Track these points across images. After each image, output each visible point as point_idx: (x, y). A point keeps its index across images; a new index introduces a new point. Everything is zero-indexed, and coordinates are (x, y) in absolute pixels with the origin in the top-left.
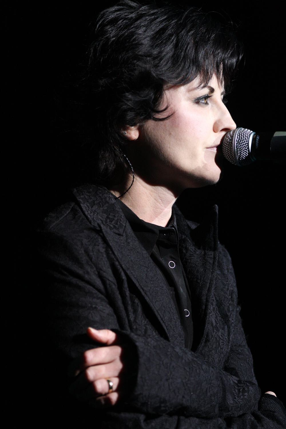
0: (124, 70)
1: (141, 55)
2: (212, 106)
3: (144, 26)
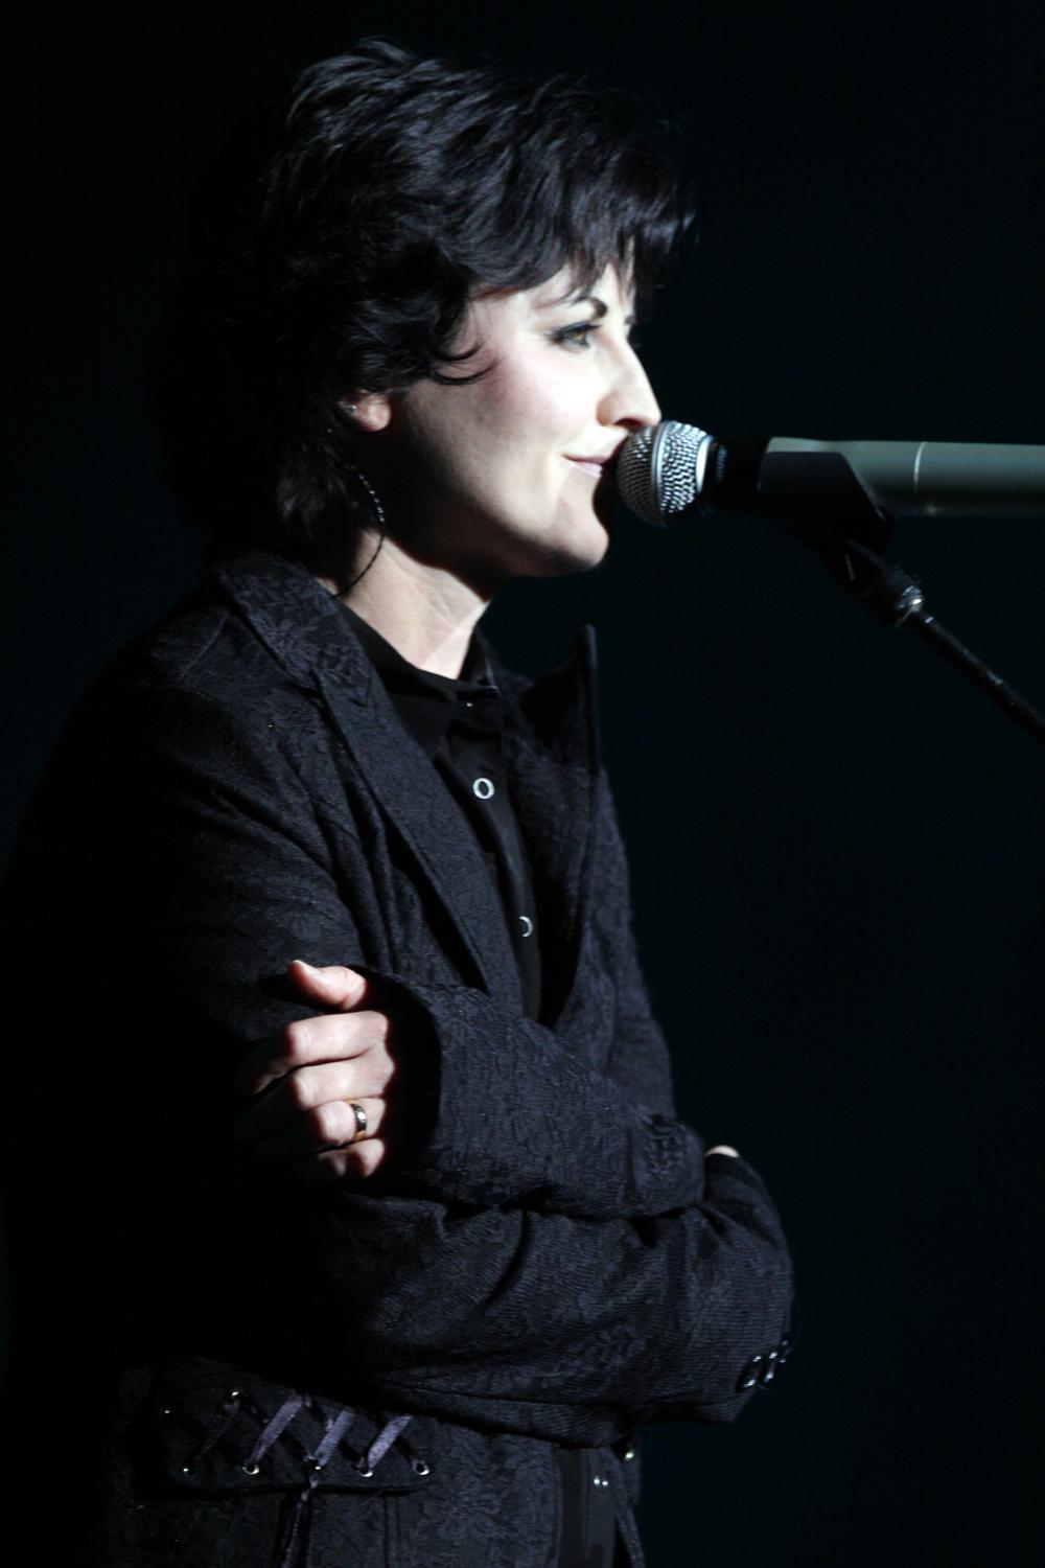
0: (364, 235)
1: (411, 198)
2: (598, 353)
3: (424, 117)
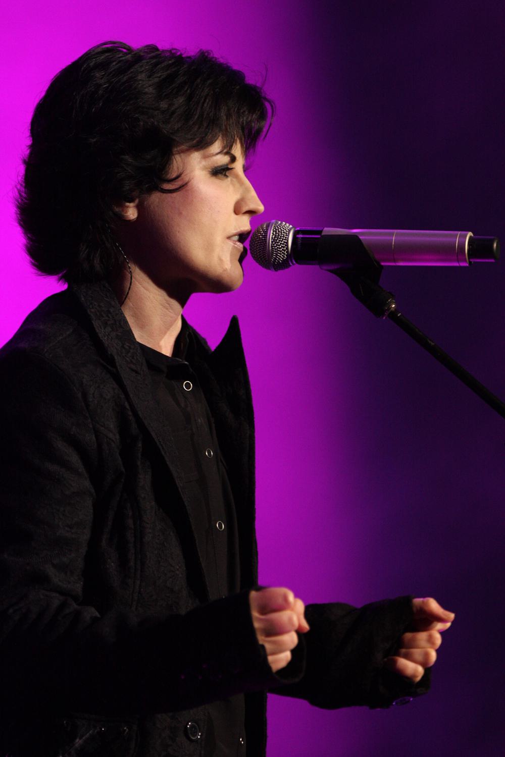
2: (231, 180)
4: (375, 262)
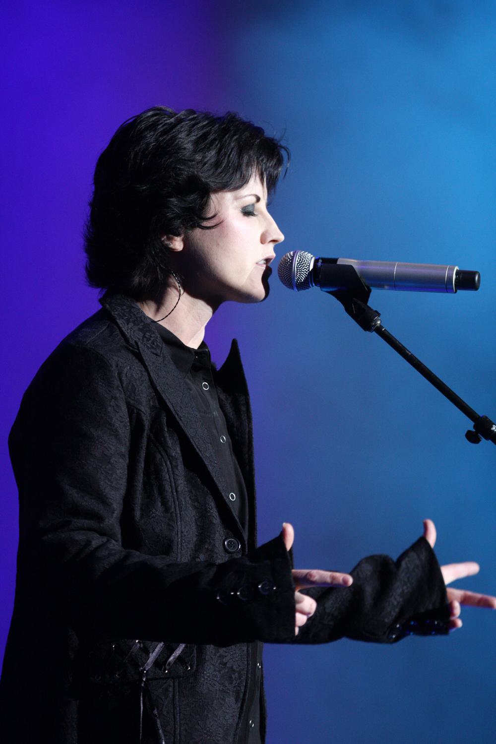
1: (186, 160)
4: (366, 288)
